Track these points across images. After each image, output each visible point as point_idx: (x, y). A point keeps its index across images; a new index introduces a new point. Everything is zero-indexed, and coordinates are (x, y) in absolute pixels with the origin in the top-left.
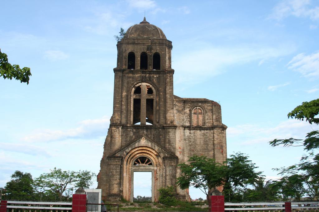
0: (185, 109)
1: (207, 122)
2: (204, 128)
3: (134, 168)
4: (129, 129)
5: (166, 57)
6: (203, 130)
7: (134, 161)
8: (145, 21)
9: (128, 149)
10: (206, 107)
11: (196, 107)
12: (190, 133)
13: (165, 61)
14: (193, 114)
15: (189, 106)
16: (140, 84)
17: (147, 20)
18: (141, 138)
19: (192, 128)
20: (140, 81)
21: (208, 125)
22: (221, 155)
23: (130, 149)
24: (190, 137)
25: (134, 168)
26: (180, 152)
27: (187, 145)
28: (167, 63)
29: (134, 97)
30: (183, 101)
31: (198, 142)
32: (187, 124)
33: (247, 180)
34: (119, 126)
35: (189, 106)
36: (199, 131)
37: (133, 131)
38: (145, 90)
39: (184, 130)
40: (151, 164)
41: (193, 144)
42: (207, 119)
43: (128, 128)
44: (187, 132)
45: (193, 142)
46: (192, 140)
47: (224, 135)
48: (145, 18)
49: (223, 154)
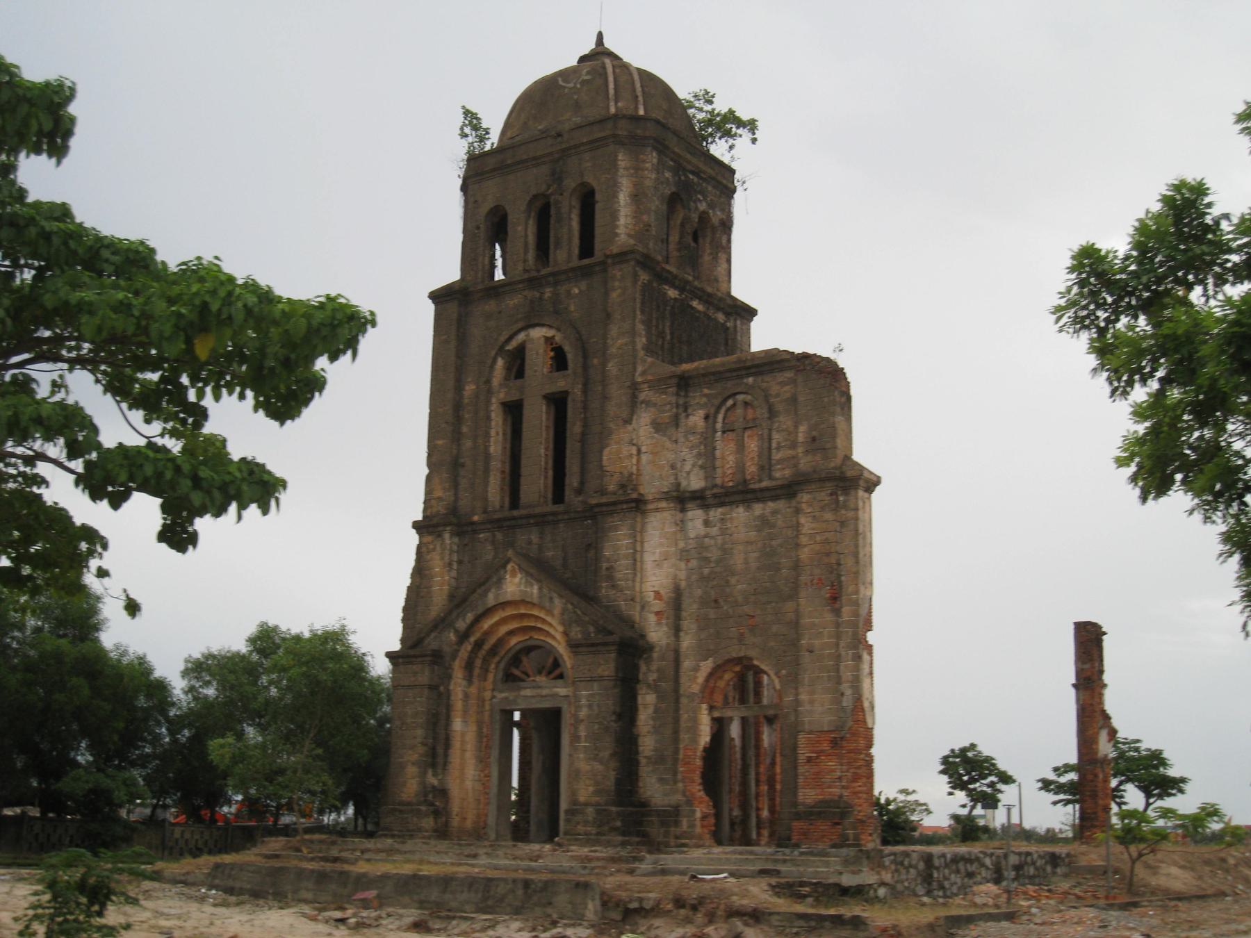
0: (687, 416)
1: (779, 462)
2: (762, 490)
3: (503, 695)
4: (481, 536)
5: (615, 196)
6: (758, 500)
7: (502, 665)
8: (600, 49)
9: (464, 620)
10: (775, 389)
11: (735, 394)
12: (707, 523)
13: (614, 216)
14: (719, 434)
15: (705, 395)
16: (521, 337)
17: (609, 44)
18: (504, 566)
19: (710, 501)
20: (520, 325)
21: (782, 474)
22: (829, 617)
23: (470, 617)
24: (706, 539)
25: (503, 695)
26: (657, 613)
27: (694, 577)
28: (622, 221)
29: (502, 395)
30: (675, 381)
31: (738, 561)
32: (695, 482)
33: (57, 570)
34: (441, 529)
35: (704, 400)
36: (741, 509)
37: (493, 542)
38: (538, 360)
39: (683, 510)
40: (561, 676)
41: (718, 569)
42: (778, 448)
43: (475, 532)
44: (696, 518)
45: (718, 562)
46: (714, 554)
47: (851, 514)
48: (600, 36)
49: (837, 612)
